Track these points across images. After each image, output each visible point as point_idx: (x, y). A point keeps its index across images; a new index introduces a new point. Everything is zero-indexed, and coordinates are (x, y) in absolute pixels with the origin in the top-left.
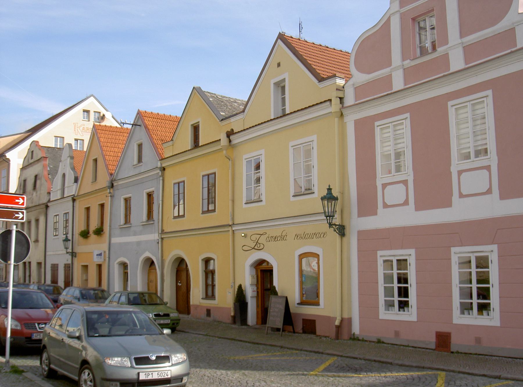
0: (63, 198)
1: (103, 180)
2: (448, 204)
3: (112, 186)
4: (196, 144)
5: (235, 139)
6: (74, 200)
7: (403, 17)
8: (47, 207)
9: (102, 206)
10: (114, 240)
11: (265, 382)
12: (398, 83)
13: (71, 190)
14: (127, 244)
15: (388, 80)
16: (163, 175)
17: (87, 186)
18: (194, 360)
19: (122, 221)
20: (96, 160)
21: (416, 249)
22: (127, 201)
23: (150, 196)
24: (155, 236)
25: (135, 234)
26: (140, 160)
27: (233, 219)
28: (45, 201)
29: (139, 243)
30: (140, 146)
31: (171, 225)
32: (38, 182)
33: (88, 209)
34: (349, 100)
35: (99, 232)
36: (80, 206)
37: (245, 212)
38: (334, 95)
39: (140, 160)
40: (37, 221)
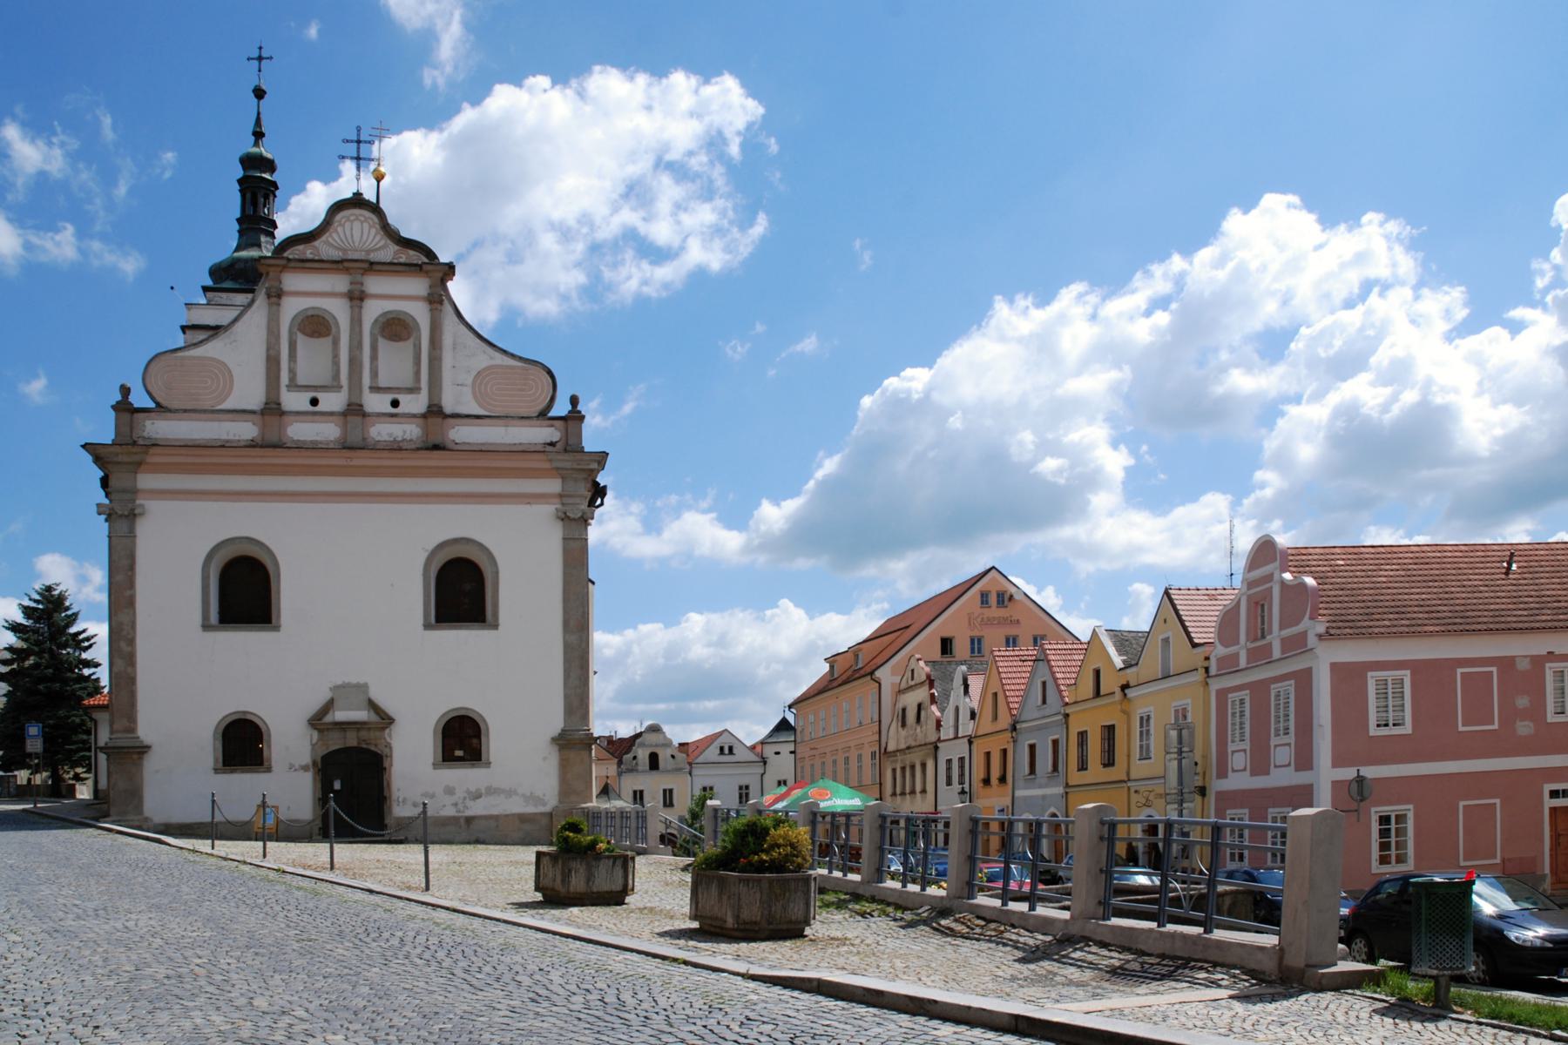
0: (956, 738)
1: (1004, 721)
2: (1267, 773)
3: (1014, 728)
4: (1097, 694)
5: (1131, 693)
6: (970, 743)
7: (1249, 597)
8: (936, 748)
9: (1005, 751)
10: (1018, 793)
11: (418, 933)
12: (1243, 663)
13: (967, 728)
14: (1031, 797)
15: (1236, 656)
16: (1067, 723)
17: (986, 725)
18: (1344, 919)
19: (1027, 770)
20: (995, 694)
21: (581, 450)
22: (1032, 747)
23: (1055, 743)
24: (1060, 790)
25: (1040, 787)
26: (1044, 702)
27: (1128, 774)
28: (933, 738)
29: (1044, 797)
30: (1044, 683)
31: (1076, 777)
32: (923, 713)
33: (988, 754)
34: (1213, 671)
35: (1003, 779)
36: (979, 748)
37: (1140, 769)
38: (1201, 663)
39: (1044, 702)
40: (924, 765)
